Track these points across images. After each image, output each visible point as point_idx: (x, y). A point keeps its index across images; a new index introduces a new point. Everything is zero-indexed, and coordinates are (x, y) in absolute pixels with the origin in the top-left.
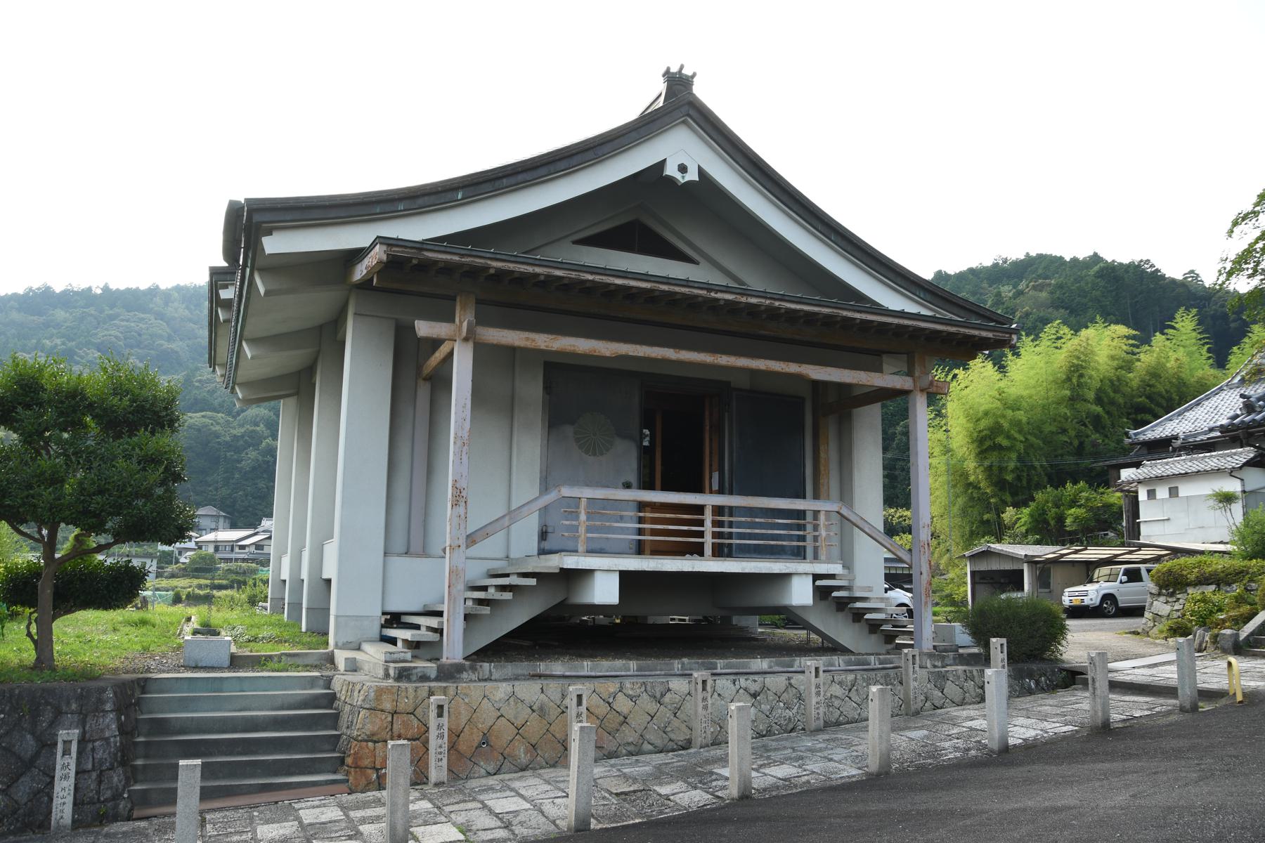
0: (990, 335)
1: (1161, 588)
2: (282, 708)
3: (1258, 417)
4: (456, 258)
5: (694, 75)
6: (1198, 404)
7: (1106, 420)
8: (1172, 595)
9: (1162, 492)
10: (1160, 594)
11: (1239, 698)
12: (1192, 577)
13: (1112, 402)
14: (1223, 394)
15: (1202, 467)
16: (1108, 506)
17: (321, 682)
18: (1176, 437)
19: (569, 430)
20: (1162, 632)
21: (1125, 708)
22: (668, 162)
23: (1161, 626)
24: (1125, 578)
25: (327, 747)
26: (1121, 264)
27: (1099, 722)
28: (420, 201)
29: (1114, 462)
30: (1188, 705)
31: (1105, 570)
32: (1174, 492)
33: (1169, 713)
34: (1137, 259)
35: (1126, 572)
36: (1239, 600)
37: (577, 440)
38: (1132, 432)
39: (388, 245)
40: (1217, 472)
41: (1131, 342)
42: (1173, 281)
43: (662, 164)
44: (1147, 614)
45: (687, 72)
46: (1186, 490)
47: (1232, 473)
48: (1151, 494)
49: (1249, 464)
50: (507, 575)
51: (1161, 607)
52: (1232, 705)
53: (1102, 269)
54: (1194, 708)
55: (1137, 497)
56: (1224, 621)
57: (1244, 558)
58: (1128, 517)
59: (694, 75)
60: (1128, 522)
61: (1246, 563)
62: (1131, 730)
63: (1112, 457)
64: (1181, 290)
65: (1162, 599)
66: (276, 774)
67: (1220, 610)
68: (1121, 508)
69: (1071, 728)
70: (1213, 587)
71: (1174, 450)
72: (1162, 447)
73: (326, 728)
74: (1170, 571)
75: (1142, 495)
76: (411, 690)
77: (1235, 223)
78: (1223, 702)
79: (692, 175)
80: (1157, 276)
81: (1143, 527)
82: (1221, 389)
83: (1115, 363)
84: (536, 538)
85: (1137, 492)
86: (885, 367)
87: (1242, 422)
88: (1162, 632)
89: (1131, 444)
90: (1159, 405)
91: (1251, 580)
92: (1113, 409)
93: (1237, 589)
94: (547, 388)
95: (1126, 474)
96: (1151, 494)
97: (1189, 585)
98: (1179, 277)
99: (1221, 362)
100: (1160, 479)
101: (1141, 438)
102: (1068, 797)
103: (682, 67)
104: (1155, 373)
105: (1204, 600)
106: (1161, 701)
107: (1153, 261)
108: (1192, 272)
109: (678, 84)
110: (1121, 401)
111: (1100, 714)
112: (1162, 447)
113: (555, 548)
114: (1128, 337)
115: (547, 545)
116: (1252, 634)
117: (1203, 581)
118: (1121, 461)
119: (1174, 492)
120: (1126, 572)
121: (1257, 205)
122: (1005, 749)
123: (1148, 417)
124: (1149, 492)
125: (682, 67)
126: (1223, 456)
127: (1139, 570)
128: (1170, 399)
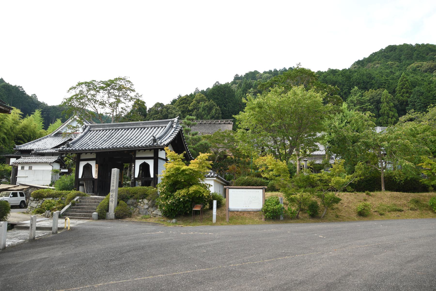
0: (3, 108)
1: (34, 198)
3: (71, 149)
6: (40, 140)
7: (7, 140)
8: (38, 200)
9: (27, 168)
10: (34, 200)
11: (69, 229)
12: (46, 195)
13: (9, 135)
14: (48, 138)
15: (41, 161)
16: (6, 170)
18: (33, 150)
20: (33, 212)
21: (39, 234)
23: (33, 211)
24: (12, 196)
26: (11, 85)
27: (32, 238)
29: (9, 155)
30: (55, 232)
31: (5, 192)
32: (30, 168)
33: (49, 234)
34: (18, 85)
35: (13, 194)
36: (60, 202)
38: (17, 146)
40: (46, 163)
41: (20, 116)
42: (28, 96)
44: (29, 207)
46: (35, 168)
47: (50, 164)
48: (23, 168)
49: (56, 162)
51: (34, 204)
52: (67, 231)
53: (4, 85)
54: (56, 233)
55: (17, 168)
56: (55, 208)
57: (61, 190)
58: (13, 175)
60: (13, 176)
61: (61, 191)
62: (41, 240)
63: (7, 154)
64: (30, 100)
65: (34, 202)
67: (54, 205)
68: (11, 171)
69: (22, 240)
70: (52, 198)
71: (32, 154)
72: (28, 153)
74: (38, 193)
75: (19, 168)
77: (70, 89)
78: (63, 231)
80: (23, 93)
81: (18, 179)
82: (48, 137)
83: (13, 122)
85: (17, 167)
87: (66, 149)
88: (33, 212)
89: (16, 150)
90: (26, 139)
91: (63, 197)
92: (10, 137)
93: (59, 199)
95: (13, 160)
96: (23, 168)
97: (44, 197)
98: (30, 95)
99: (46, 127)
100: (27, 163)
101: (20, 148)
102: (43, 255)
104: (25, 128)
105: (49, 202)
106: (45, 231)
107: (23, 87)
108: (35, 95)
110: (13, 135)
111: (33, 235)
112: (28, 153)
114: (20, 114)
116: (64, 212)
117: (49, 196)
118: (11, 155)
119: (30, 168)
120: (13, 194)
121: (77, 85)
122: (5, 248)
123: (22, 142)
124: (22, 167)
126: (47, 158)
127: (17, 193)
128: (30, 137)
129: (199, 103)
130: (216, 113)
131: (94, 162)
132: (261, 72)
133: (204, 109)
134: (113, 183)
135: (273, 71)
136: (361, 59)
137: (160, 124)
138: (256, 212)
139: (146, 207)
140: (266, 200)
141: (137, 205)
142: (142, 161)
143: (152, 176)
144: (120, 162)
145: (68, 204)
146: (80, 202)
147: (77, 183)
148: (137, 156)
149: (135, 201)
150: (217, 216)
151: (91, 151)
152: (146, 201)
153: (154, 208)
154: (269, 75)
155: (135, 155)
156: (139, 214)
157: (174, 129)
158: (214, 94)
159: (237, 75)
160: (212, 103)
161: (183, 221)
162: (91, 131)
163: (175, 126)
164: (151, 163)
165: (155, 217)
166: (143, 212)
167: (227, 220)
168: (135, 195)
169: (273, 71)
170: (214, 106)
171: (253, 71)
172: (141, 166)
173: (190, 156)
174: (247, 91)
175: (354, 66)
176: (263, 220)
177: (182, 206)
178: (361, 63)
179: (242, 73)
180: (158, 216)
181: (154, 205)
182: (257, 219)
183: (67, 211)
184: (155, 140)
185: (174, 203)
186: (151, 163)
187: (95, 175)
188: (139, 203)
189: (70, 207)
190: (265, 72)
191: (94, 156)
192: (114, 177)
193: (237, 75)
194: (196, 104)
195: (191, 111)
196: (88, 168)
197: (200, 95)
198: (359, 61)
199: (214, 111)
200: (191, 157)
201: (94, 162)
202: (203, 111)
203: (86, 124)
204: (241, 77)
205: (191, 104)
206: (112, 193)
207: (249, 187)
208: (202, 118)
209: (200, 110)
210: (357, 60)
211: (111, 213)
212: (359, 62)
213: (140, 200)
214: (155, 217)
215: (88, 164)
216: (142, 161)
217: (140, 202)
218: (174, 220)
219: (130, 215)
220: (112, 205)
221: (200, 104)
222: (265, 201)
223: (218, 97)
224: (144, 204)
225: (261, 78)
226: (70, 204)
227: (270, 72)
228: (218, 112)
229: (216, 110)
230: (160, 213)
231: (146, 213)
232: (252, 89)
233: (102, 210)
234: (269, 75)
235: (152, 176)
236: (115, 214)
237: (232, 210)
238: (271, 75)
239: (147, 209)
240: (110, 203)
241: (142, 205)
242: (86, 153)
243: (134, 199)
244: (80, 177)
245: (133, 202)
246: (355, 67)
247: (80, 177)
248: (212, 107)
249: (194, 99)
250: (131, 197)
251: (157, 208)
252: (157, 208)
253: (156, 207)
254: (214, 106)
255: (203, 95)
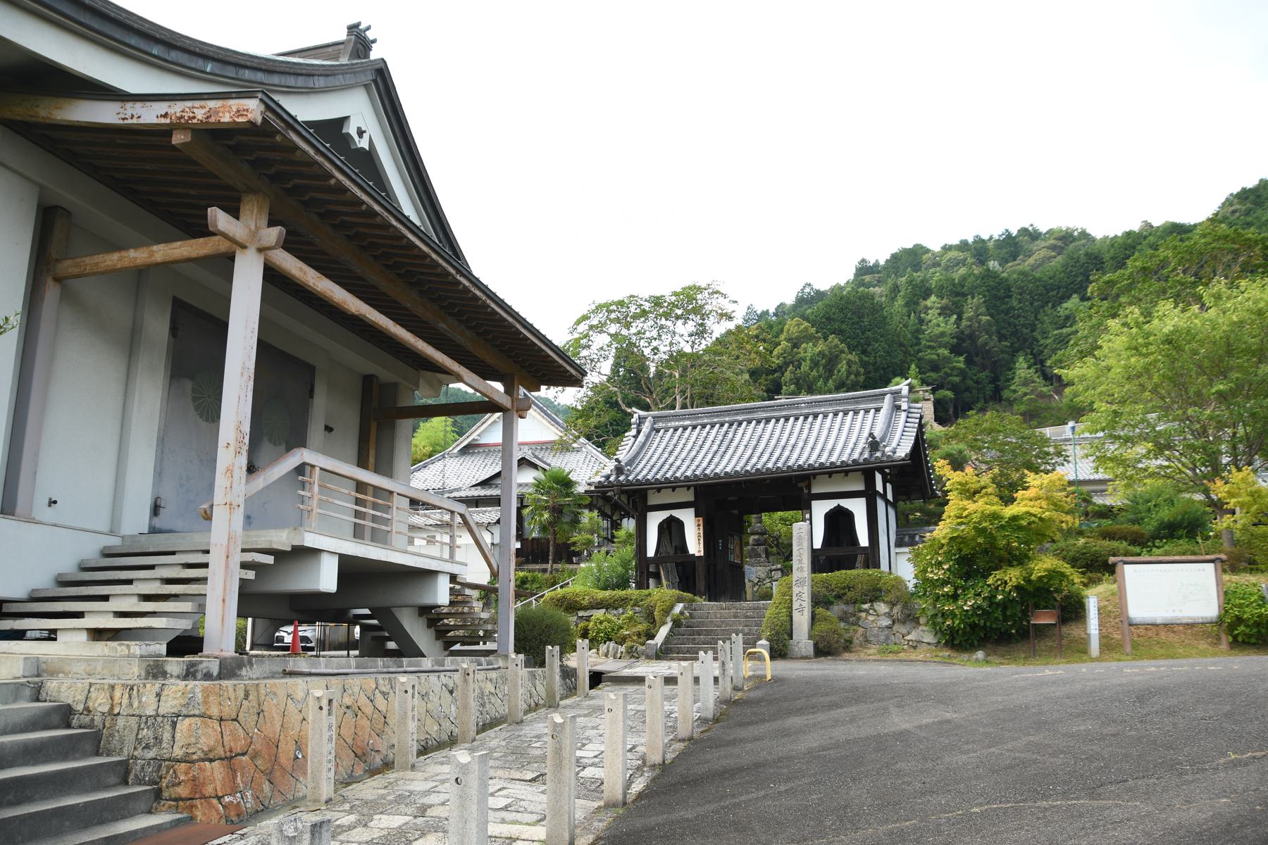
2: (14, 731)
4: (312, 152)
5: (374, 41)
17: (27, 692)
19: (188, 385)
22: (352, 119)
25: (113, 779)
28: (174, 55)
37: (194, 400)
39: (268, 107)
43: (343, 121)
45: (370, 35)
50: (173, 553)
59: (374, 41)
66: (102, 822)
73: (85, 755)
76: (231, 689)
79: (363, 144)
82: (443, 457)
84: (147, 511)
86: (421, 382)
94: (174, 329)
103: (368, 28)
109: (359, 41)
113: (165, 527)
115: (158, 522)
125: (368, 28)
129: (796, 345)
130: (849, 373)
131: (691, 511)
132: (936, 247)
133: (815, 364)
134: (800, 561)
135: (970, 240)
136: (1251, 183)
137: (858, 403)
138: (1191, 627)
139: (886, 622)
140: (1226, 593)
141: (859, 619)
142: (830, 505)
143: (864, 541)
144: (736, 512)
145: (664, 623)
146: (691, 616)
147: (646, 571)
148: (815, 490)
149: (850, 609)
150: (1102, 637)
151: (673, 484)
152: (882, 608)
153: (909, 625)
154: (961, 255)
155: (809, 487)
156: (867, 641)
157: (904, 415)
158: (828, 319)
159: (863, 260)
160: (836, 346)
161: (1003, 656)
162: (658, 431)
163: (905, 406)
164: (858, 508)
165: (915, 648)
166: (877, 636)
167: (1128, 649)
168: (850, 594)
169: (970, 240)
170: (842, 352)
171: (910, 246)
172: (661, 526)
173: (932, 485)
174: (917, 303)
175: (1231, 209)
176: (1224, 646)
177: (998, 614)
178: (1252, 197)
179: (880, 255)
180: (925, 647)
181: (911, 618)
182: (1203, 645)
183: (667, 640)
184: (874, 445)
185: (979, 607)
186: (858, 508)
187: (694, 544)
188: (863, 615)
189: (671, 630)
190: (947, 248)
191: (689, 496)
192: (800, 544)
193: (863, 260)
194: (789, 350)
195: (775, 371)
196: (672, 530)
197: (798, 325)
198: (1244, 191)
199: (843, 367)
200: (933, 491)
201: (691, 511)
202: (811, 369)
203: (642, 413)
204: (876, 265)
205: (775, 352)
206: (800, 589)
207: (1183, 558)
208: (810, 391)
209: (805, 367)
210: (1236, 190)
211: (802, 638)
212: (1244, 195)
213: (866, 606)
214: (915, 648)
215: (672, 519)
216: (830, 505)
217: (866, 611)
218: (980, 654)
219: (848, 646)
220: (802, 620)
221: (801, 350)
222: (1226, 596)
223: (844, 327)
224: (879, 615)
225: (939, 265)
226: (669, 625)
227: (964, 246)
228: (854, 368)
229: (849, 363)
230: (929, 638)
231: (887, 638)
232: (933, 298)
233: (777, 633)
234: (961, 255)
235: (864, 541)
236: (816, 646)
237: (1137, 621)
238: (967, 254)
239: (889, 627)
240: (796, 615)
241: (871, 618)
242: (659, 490)
243: (847, 603)
244: (651, 552)
245: (845, 613)
246: (1234, 212)
247: (651, 552)
248: (837, 356)
249: (782, 337)
250: (839, 597)
251: (918, 623)
252: (918, 623)
253: (916, 621)
254: (842, 352)
255: (806, 324)
